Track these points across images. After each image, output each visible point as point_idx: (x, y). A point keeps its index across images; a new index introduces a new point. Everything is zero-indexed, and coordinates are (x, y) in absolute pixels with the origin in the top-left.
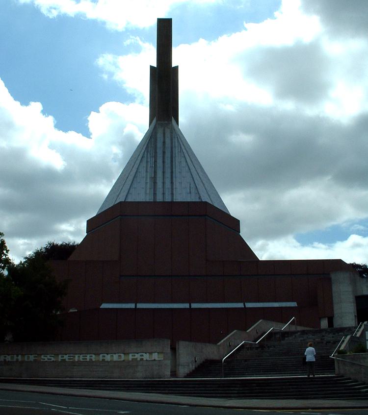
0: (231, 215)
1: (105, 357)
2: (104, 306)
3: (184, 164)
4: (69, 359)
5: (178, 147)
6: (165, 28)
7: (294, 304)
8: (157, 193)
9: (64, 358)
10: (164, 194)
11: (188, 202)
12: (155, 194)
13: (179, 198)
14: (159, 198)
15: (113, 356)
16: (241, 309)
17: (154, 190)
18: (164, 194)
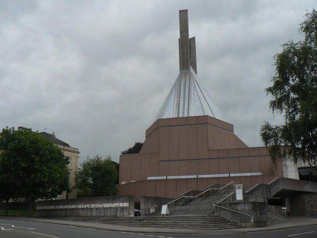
2: (149, 178)
3: (196, 94)
6: (184, 16)
7: (259, 174)
8: (180, 112)
12: (178, 113)
13: (192, 115)
14: (181, 115)
16: (227, 177)
18: (184, 113)
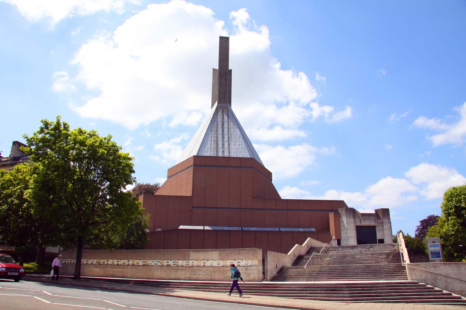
0: (264, 167)
1: (205, 263)
2: (181, 227)
4: (174, 264)
5: (232, 118)
9: (169, 263)
10: (223, 152)
11: (241, 158)
12: (217, 152)
13: (233, 155)
14: (220, 155)
15: (137, 264)
17: (217, 150)
